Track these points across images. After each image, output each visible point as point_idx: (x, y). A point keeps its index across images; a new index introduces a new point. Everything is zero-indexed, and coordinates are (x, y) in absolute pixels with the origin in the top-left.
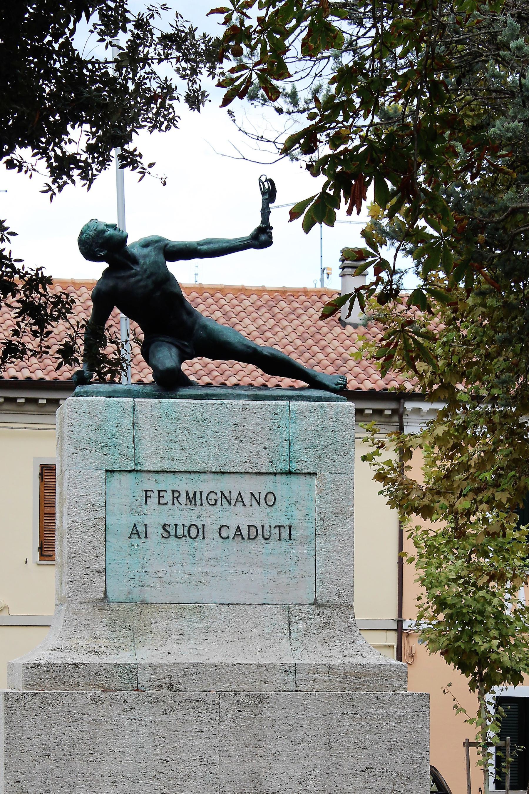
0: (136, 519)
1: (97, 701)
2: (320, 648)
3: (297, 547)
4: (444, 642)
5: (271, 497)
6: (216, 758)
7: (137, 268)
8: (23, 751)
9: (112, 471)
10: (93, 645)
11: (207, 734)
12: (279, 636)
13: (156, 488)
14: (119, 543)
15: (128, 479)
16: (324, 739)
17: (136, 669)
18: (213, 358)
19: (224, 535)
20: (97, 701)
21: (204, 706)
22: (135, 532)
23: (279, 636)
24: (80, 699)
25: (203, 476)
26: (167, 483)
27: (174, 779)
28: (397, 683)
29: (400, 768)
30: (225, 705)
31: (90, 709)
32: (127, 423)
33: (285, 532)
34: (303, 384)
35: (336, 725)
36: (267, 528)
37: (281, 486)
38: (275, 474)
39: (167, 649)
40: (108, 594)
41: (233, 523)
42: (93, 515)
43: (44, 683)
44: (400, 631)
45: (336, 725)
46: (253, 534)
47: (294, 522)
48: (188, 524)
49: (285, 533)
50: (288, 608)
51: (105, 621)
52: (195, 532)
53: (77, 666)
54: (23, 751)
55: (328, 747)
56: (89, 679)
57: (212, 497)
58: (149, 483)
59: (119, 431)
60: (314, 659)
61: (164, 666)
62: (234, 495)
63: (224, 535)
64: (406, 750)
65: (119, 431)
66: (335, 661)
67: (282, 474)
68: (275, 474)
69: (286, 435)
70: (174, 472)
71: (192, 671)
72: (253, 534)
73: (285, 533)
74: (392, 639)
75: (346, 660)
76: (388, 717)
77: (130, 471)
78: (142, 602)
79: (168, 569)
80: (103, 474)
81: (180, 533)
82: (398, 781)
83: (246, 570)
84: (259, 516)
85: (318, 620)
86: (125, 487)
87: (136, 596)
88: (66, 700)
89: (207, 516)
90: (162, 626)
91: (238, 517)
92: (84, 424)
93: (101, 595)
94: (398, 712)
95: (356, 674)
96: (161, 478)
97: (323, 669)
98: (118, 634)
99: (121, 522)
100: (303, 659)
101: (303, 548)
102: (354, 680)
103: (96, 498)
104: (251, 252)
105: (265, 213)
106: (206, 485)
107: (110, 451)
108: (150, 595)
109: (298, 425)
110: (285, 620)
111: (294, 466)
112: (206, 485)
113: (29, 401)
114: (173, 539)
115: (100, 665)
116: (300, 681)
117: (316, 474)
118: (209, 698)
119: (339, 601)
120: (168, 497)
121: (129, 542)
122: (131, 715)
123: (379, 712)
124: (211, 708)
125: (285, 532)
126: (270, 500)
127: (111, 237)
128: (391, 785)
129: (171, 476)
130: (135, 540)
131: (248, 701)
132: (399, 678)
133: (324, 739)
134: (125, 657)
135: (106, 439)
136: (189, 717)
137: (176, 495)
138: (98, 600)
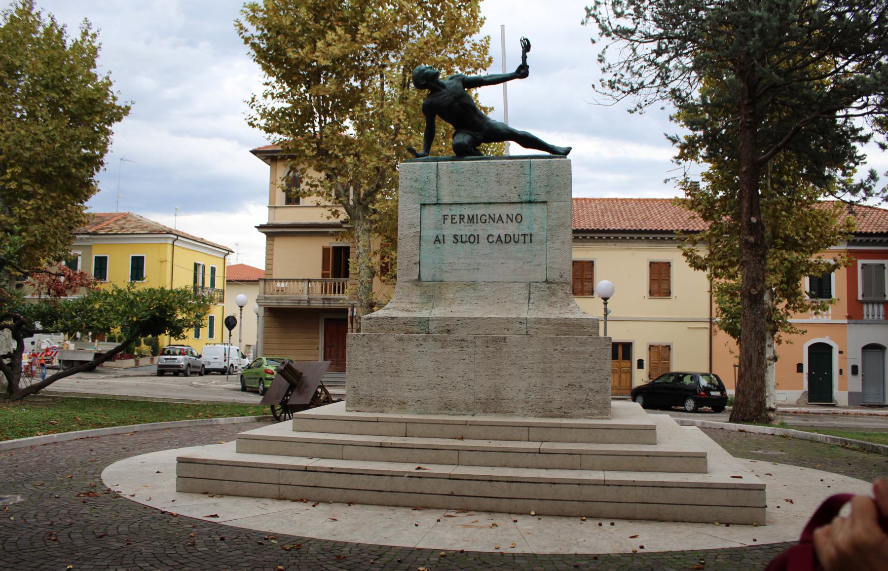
0: (439, 232)
1: (400, 339)
2: (546, 308)
3: (536, 247)
4: (725, 325)
5: (519, 217)
6: (472, 376)
7: (444, 91)
8: (356, 369)
9: (424, 205)
10: (409, 306)
11: (467, 361)
12: (522, 301)
13: (450, 213)
15: (434, 209)
16: (542, 366)
17: (427, 320)
18: (499, 141)
19: (490, 240)
20: (400, 339)
21: (465, 344)
22: (437, 240)
23: (522, 301)
26: (456, 211)
27: (446, 388)
28: (591, 330)
29: (591, 386)
30: (478, 343)
33: (528, 238)
34: (547, 154)
35: (549, 357)
36: (516, 236)
37: (525, 210)
38: (522, 203)
41: (496, 233)
42: (413, 230)
44: (711, 322)
45: (549, 357)
46: (509, 239)
47: (533, 232)
48: (469, 234)
49: (528, 238)
50: (529, 285)
51: (418, 293)
52: (473, 239)
53: (393, 318)
54: (356, 369)
55: (544, 371)
57: (484, 218)
58: (446, 211)
59: (429, 181)
60: (541, 315)
61: (444, 319)
62: (497, 216)
63: (490, 240)
64: (595, 374)
66: (553, 317)
67: (526, 203)
68: (522, 203)
69: (528, 179)
70: (461, 204)
71: (463, 322)
72: (509, 239)
73: (528, 238)
74: (708, 325)
75: (560, 316)
76: (583, 352)
77: (435, 204)
78: (442, 281)
79: (457, 262)
80: (419, 207)
81: (464, 240)
83: (503, 261)
84: (511, 229)
85: (547, 292)
86: (432, 214)
87: (438, 278)
88: (382, 339)
89: (480, 230)
90: (451, 295)
91: (499, 230)
93: (416, 277)
94: (590, 349)
95: (565, 324)
96: (453, 207)
99: (429, 233)
100: (532, 315)
101: (538, 248)
102: (564, 328)
105: (524, 58)
106: (480, 211)
107: (423, 193)
108: (446, 277)
109: (535, 173)
111: (533, 198)
112: (480, 211)
113: (615, 238)
114: (460, 244)
115: (407, 318)
116: (528, 328)
119: (561, 280)
120: (457, 219)
122: (421, 348)
123: (578, 349)
124: (470, 345)
125: (528, 238)
126: (519, 219)
127: (428, 73)
128: (585, 396)
130: (438, 245)
132: (594, 327)
133: (542, 366)
134: (425, 314)
135: (421, 186)
136: (456, 350)
137: (462, 217)
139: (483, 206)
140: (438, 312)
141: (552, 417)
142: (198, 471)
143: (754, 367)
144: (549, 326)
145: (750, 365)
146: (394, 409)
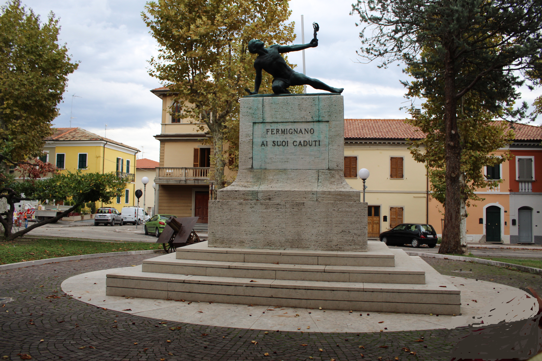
1: (241, 204)
2: (329, 185)
5: (312, 130)
6: (284, 226)
10: (246, 184)
12: (314, 181)
13: (270, 128)
14: (257, 148)
15: (261, 126)
16: (326, 220)
17: (257, 192)
18: (300, 85)
19: (295, 144)
20: (241, 204)
21: (280, 207)
22: (263, 144)
23: (314, 181)
24: (235, 203)
25: (288, 124)
26: (275, 126)
27: (268, 233)
29: (356, 232)
30: (288, 206)
31: (238, 207)
32: (260, 106)
33: (318, 143)
36: (311, 142)
37: (316, 126)
38: (314, 122)
39: (271, 186)
40: (254, 166)
41: (298, 140)
42: (248, 138)
43: (225, 197)
44: (427, 194)
46: (306, 144)
48: (282, 141)
50: (318, 171)
51: (252, 176)
52: (285, 144)
53: (236, 191)
55: (327, 223)
56: (240, 196)
58: (268, 127)
59: (258, 109)
60: (325, 189)
62: (299, 130)
63: (295, 144)
64: (358, 225)
65: (258, 109)
66: (332, 190)
67: (316, 122)
68: (314, 122)
69: (317, 107)
70: (277, 123)
71: (278, 193)
73: (317, 143)
74: (426, 195)
75: (337, 190)
76: (351, 211)
78: (265, 169)
81: (279, 144)
82: (355, 236)
83: (303, 157)
84: (308, 137)
85: (329, 175)
86: (260, 128)
87: (263, 167)
88: (230, 203)
89: (289, 138)
90: (271, 177)
91: (300, 138)
92: (246, 107)
93: (250, 167)
94: (355, 209)
95: (340, 195)
96: (272, 125)
97: (327, 193)
98: (255, 181)
99: (258, 140)
100: (320, 189)
101: (324, 149)
102: (339, 197)
103: (249, 132)
104: (311, 48)
105: (315, 35)
106: (288, 127)
107: (254, 116)
108: (268, 166)
109: (322, 104)
110: (317, 175)
111: (321, 119)
112: (288, 127)
115: (244, 191)
117: (328, 121)
118: (282, 203)
119: (337, 168)
120: (275, 131)
121: (261, 148)
122: (253, 209)
123: (347, 209)
124: (282, 207)
126: (312, 131)
127: (257, 44)
128: (352, 238)
129: (276, 124)
130: (263, 147)
131: (297, 205)
132: (357, 196)
133: (326, 220)
134: (255, 188)
135: (253, 112)
136: (274, 210)
137: (278, 131)
138: (250, 168)
139: (290, 123)
140: (263, 187)
141: (332, 250)
142: (119, 283)
143: (453, 220)
144: (330, 196)
145: (451, 219)
146: (237, 246)
